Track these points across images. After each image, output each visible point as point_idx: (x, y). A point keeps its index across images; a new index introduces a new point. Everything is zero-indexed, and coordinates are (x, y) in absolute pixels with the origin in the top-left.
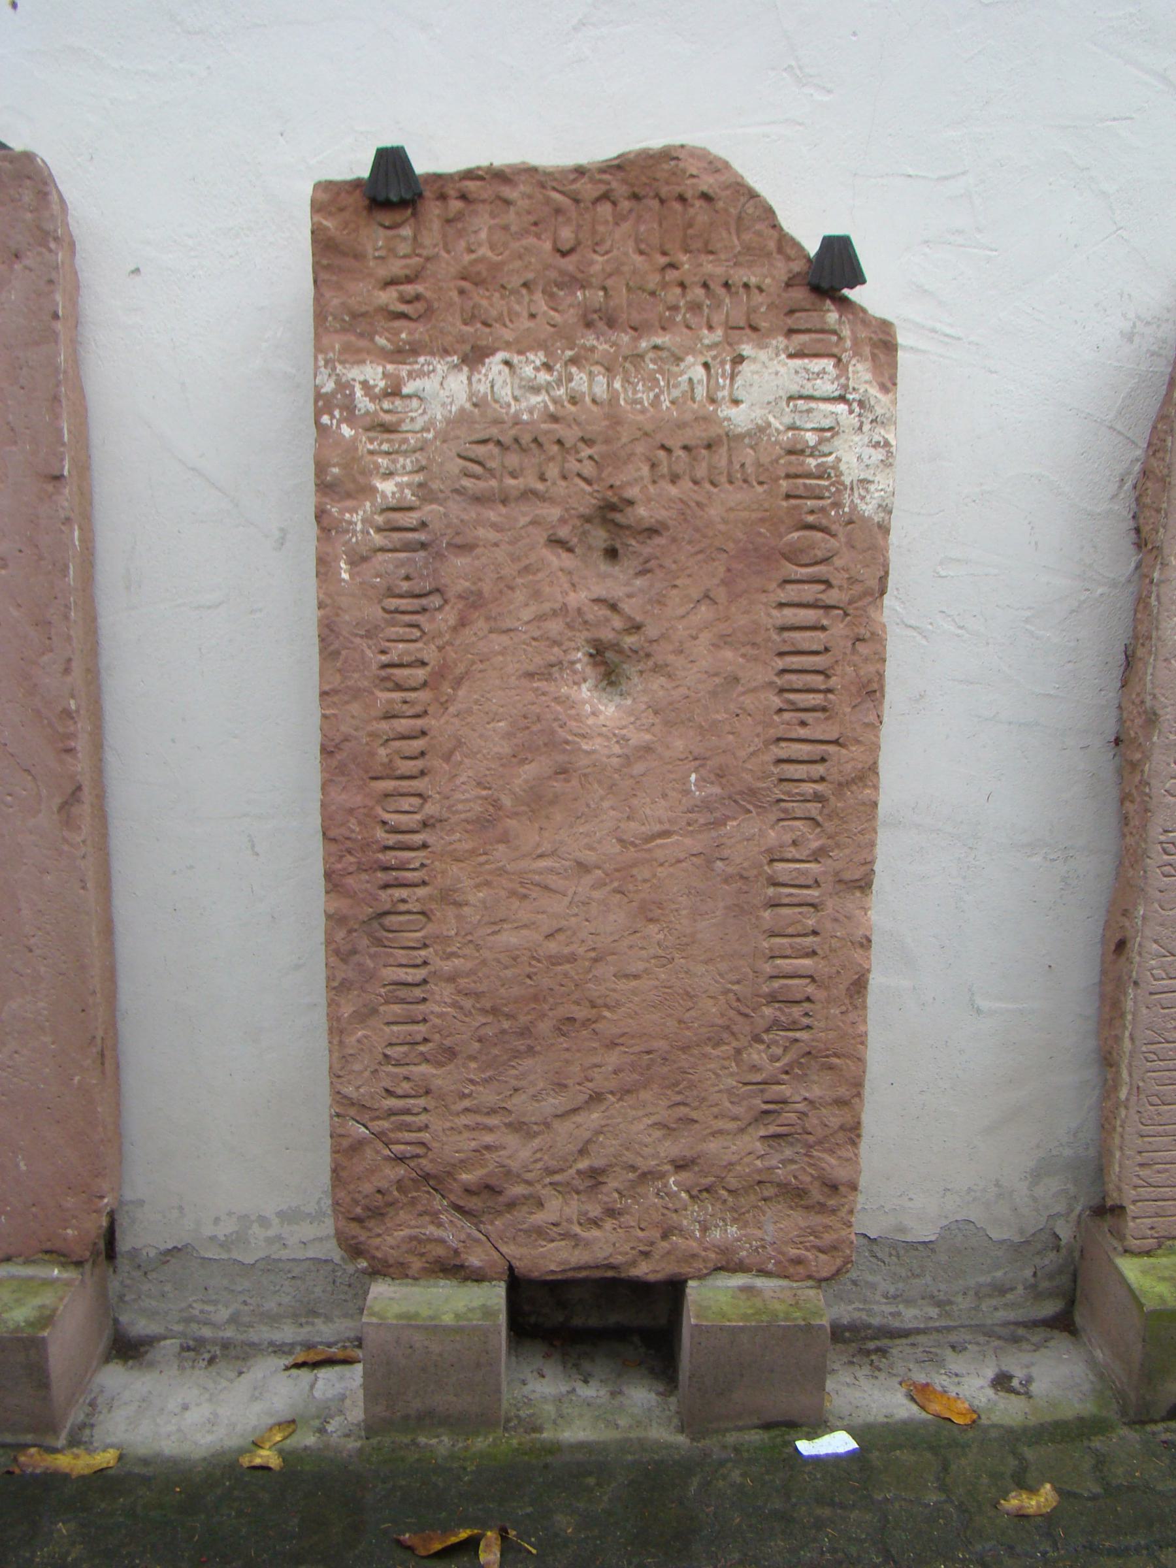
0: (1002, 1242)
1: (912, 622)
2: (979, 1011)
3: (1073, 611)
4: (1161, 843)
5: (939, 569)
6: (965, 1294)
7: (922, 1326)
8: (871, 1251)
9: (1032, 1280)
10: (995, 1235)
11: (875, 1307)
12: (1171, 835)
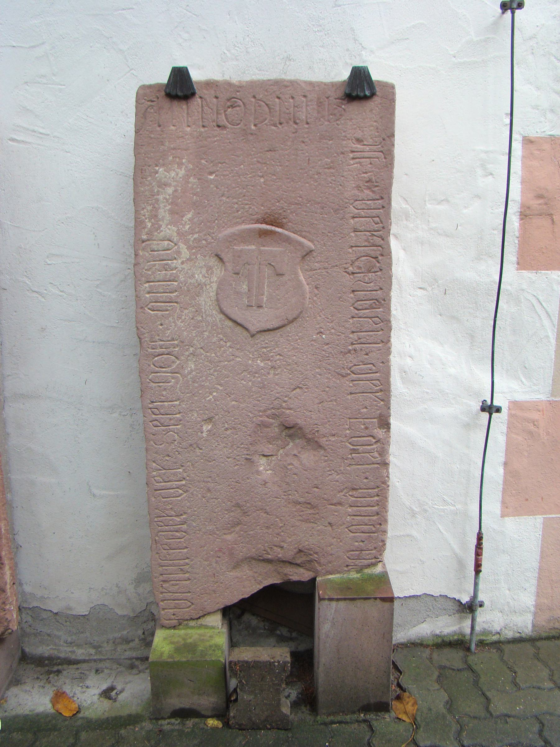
0: (124, 616)
1: (36, 289)
2: (94, 495)
3: (122, 281)
4: (151, 408)
5: (47, 260)
6: (107, 642)
7: (87, 658)
8: (56, 619)
9: (143, 636)
10: (120, 613)
11: (61, 648)
12: (155, 404)
